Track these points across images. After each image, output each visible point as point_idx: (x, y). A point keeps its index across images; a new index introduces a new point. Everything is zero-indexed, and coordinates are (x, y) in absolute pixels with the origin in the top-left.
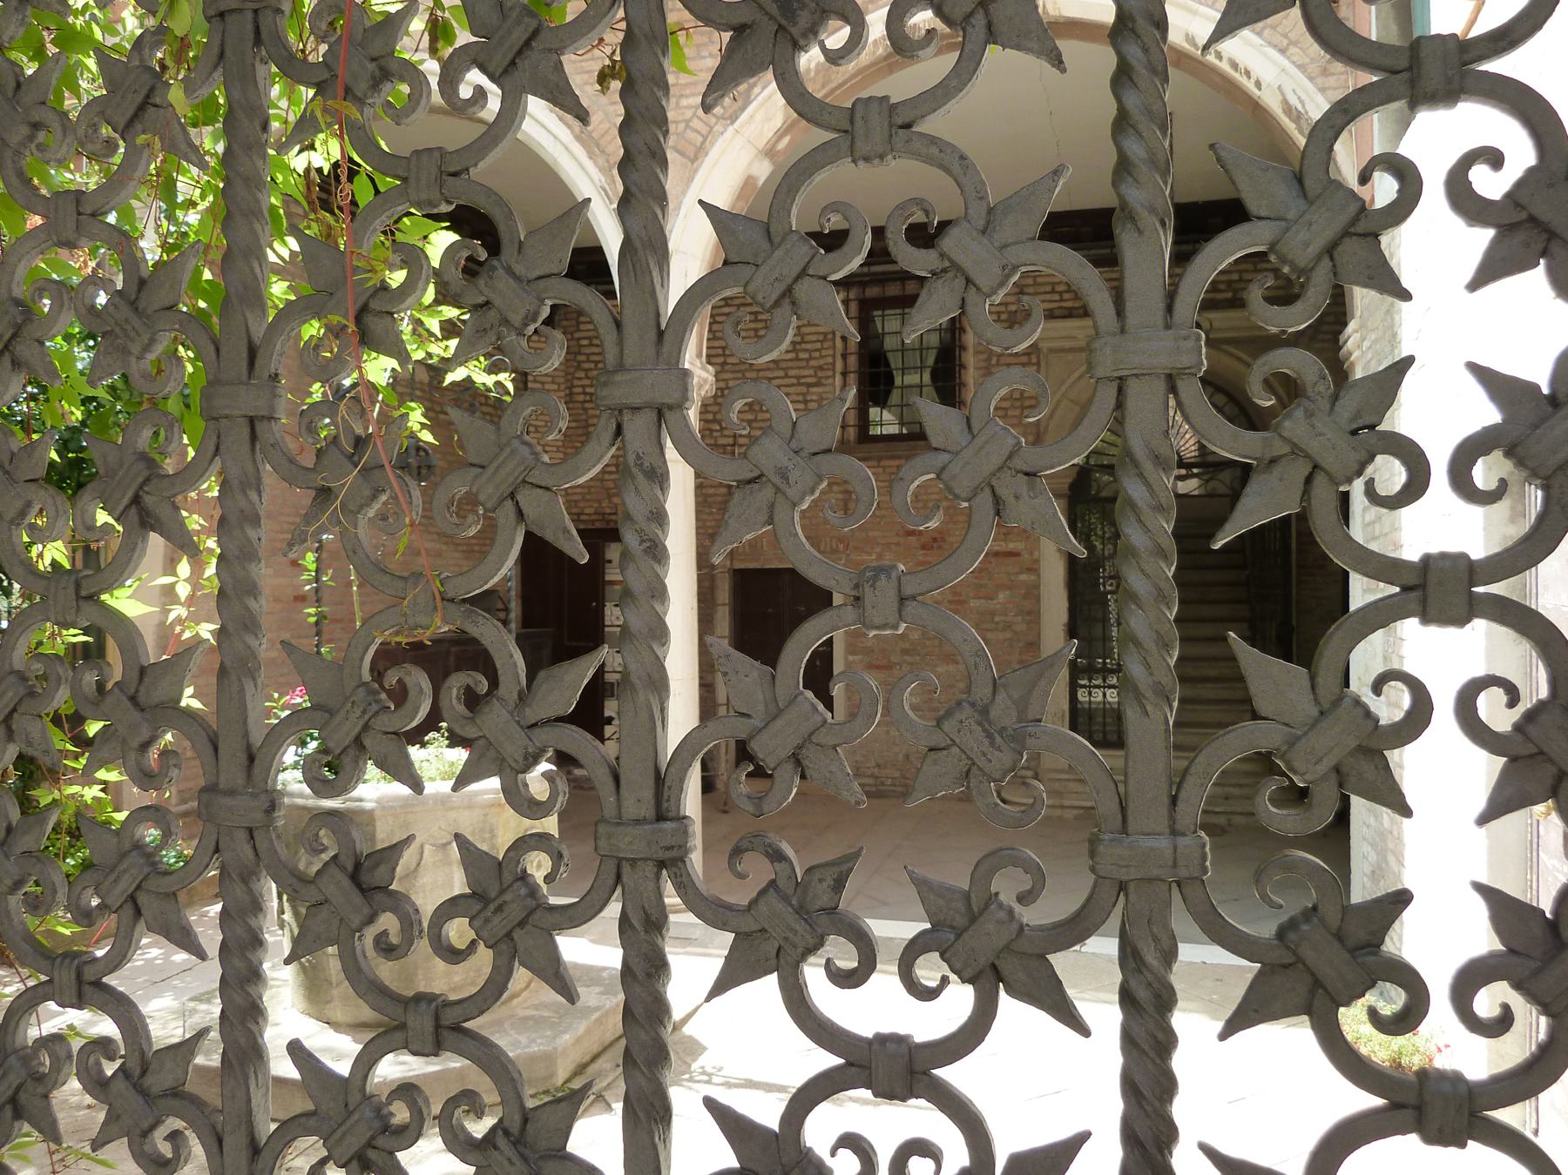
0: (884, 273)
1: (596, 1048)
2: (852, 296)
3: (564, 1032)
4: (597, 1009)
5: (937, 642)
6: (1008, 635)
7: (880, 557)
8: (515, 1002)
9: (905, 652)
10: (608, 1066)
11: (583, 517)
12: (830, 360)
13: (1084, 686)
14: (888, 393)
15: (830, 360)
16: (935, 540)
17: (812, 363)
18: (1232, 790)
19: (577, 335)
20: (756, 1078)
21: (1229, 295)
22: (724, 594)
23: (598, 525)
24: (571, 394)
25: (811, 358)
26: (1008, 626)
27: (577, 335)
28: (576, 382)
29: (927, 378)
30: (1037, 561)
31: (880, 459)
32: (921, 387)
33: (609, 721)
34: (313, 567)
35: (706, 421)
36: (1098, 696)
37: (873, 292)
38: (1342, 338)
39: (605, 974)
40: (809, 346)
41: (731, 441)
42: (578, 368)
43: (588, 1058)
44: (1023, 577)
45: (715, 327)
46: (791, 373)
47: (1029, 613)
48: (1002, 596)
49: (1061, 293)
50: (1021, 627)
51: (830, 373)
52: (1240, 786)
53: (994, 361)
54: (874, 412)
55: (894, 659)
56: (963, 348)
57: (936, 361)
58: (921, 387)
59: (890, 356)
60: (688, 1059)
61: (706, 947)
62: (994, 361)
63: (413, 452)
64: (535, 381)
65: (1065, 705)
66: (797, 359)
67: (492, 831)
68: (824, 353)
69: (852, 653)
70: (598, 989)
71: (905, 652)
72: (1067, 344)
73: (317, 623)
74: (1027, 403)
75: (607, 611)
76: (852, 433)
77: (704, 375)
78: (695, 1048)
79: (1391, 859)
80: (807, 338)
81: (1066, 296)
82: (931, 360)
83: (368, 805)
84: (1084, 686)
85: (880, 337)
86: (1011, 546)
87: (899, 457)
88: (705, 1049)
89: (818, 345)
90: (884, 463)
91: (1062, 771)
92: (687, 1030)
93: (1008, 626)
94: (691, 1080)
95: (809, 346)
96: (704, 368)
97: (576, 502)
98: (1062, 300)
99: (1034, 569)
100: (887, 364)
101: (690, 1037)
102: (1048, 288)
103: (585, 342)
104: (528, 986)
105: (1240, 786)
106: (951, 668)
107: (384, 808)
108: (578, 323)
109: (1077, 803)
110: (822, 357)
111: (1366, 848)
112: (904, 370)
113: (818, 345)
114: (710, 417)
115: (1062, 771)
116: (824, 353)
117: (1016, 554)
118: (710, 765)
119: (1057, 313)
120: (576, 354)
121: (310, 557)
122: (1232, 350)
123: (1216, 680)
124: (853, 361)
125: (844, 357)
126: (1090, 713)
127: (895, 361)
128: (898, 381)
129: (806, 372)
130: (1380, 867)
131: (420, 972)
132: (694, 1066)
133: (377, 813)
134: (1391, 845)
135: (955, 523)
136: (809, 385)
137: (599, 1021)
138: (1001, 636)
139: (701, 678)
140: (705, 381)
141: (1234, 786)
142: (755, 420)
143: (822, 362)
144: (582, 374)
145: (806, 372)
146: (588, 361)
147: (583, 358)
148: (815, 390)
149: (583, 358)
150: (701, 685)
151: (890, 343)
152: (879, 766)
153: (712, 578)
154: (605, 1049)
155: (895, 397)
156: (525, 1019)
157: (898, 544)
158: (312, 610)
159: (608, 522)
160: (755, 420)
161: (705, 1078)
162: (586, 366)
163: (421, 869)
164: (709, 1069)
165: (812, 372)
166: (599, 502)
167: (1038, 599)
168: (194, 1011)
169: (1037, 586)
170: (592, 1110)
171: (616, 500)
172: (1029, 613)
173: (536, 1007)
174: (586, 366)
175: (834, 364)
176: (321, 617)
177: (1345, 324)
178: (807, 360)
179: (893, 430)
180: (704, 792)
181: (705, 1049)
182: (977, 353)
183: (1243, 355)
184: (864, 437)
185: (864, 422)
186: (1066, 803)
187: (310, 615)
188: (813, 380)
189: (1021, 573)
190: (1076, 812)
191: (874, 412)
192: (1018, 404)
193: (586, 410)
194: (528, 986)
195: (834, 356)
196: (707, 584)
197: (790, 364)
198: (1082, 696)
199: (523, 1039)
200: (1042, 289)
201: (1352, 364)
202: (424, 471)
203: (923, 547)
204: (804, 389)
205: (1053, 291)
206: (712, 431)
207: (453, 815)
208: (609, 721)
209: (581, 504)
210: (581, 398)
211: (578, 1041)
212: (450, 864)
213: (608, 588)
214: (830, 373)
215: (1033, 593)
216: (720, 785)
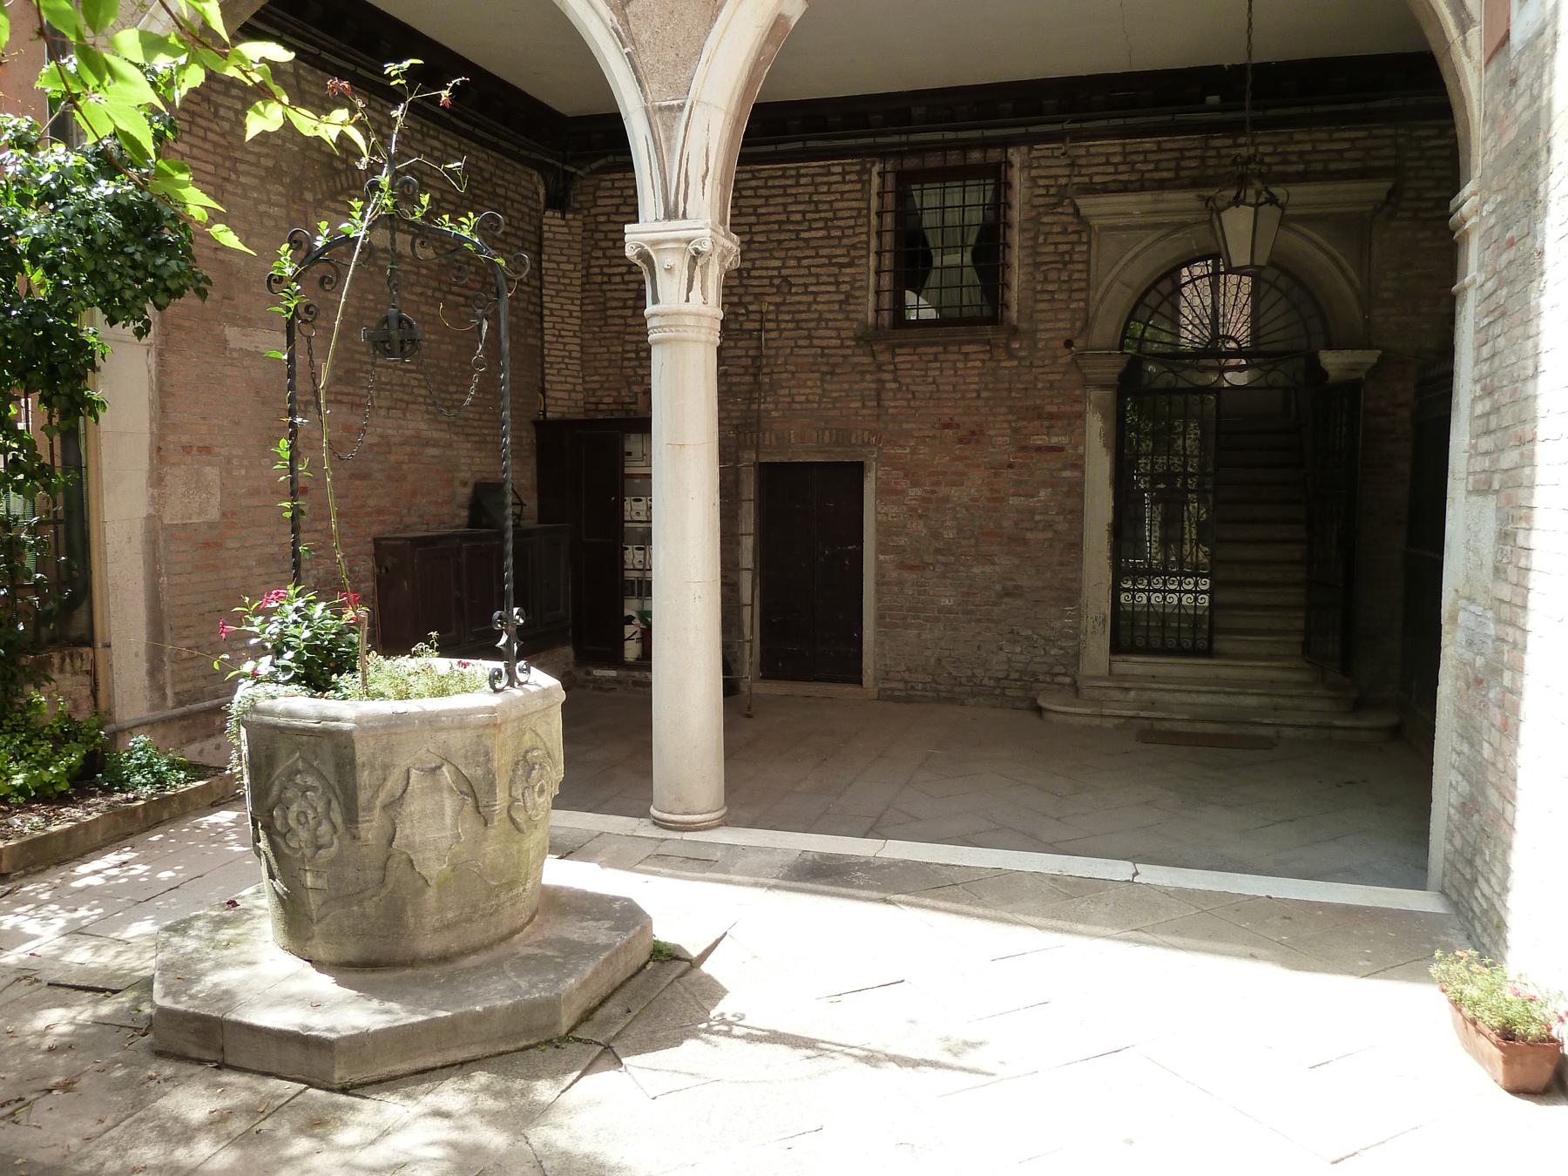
0: (924, 142)
1: (604, 991)
2: (889, 167)
3: (569, 976)
4: (606, 947)
5: (973, 541)
6: (1050, 535)
7: (914, 451)
8: (517, 937)
9: (938, 551)
10: (618, 1011)
11: (602, 407)
12: (864, 238)
13: (1127, 590)
14: (925, 275)
15: (864, 238)
16: (973, 433)
17: (845, 241)
18: (1281, 701)
19: (593, 211)
20: (783, 1028)
21: (1301, 167)
22: (749, 489)
23: (616, 415)
24: (588, 275)
25: (844, 236)
26: (1049, 525)
27: (593, 211)
28: (593, 262)
29: (968, 258)
30: (1082, 457)
31: (916, 345)
32: (962, 267)
33: (630, 620)
34: (287, 455)
35: (731, 304)
36: (1156, 598)
37: (911, 163)
38: (1453, 204)
39: (617, 906)
40: (841, 223)
41: (757, 325)
42: (596, 247)
43: (596, 1002)
44: (1066, 474)
45: (741, 202)
46: (822, 252)
47: (1071, 512)
48: (1043, 494)
49: (1115, 165)
50: (1062, 527)
51: (863, 252)
52: (1291, 696)
53: (1041, 240)
54: (911, 298)
55: (929, 559)
56: (1008, 225)
57: (979, 240)
58: (962, 267)
59: (929, 233)
60: (706, 1004)
61: (728, 872)
62: (1041, 240)
63: (394, 323)
64: (549, 261)
65: (1107, 609)
66: (829, 237)
67: (487, 754)
68: (858, 230)
69: (883, 553)
70: (607, 924)
71: (938, 551)
72: (1122, 221)
73: (293, 518)
74: (1076, 286)
75: (627, 506)
76: (886, 317)
77: (729, 244)
78: (714, 991)
79: (1493, 794)
80: (840, 214)
81: (1122, 168)
82: (972, 240)
83: (347, 726)
84: (1127, 590)
85: (917, 214)
86: (1054, 440)
87: (936, 344)
88: (725, 992)
89: (852, 222)
90: (921, 350)
91: (1102, 678)
92: (706, 968)
93: (1049, 525)
94: (708, 1031)
95: (841, 223)
96: (727, 237)
97: (594, 390)
98: (1116, 173)
99: (1078, 464)
100: (925, 243)
101: (709, 977)
102: (1103, 160)
103: (602, 219)
104: (531, 919)
105: (1291, 696)
106: (988, 569)
107: (363, 729)
108: (595, 199)
109: (1118, 712)
110: (855, 235)
111: (1454, 777)
112: (944, 250)
113: (852, 222)
114: (735, 299)
115: (1102, 678)
116: (858, 230)
117: (1058, 449)
118: (733, 667)
119: (1112, 186)
120: (593, 231)
121: (284, 444)
122: (1305, 230)
123: (1266, 584)
124: (888, 238)
125: (879, 234)
126: (1133, 616)
127: (933, 239)
128: (937, 262)
129: (839, 252)
130: (1473, 799)
131: (409, 908)
132: (714, 1013)
133: (355, 734)
134: (1492, 778)
135: (994, 415)
136: (841, 266)
137: (608, 961)
138: (1041, 536)
139: (722, 576)
140: (730, 251)
141: (1284, 696)
142: (783, 303)
143: (856, 240)
144: (600, 253)
145: (839, 252)
146: (606, 239)
147: (601, 236)
148: (848, 270)
149: (601, 236)
150: (723, 584)
151: (930, 219)
152: (909, 670)
153: (737, 472)
154: (615, 991)
155: (933, 278)
156: (528, 957)
157: (933, 437)
158: (287, 504)
159: (628, 412)
160: (783, 303)
161: (725, 1028)
162: (604, 244)
163: (407, 797)
164: (729, 1018)
165: (844, 251)
166: (618, 390)
167: (1081, 496)
168: (165, 945)
169: (1080, 483)
170: (601, 1063)
171: (635, 388)
172: (1071, 512)
173: (539, 945)
174: (604, 244)
175: (868, 243)
176: (297, 512)
177: (1456, 189)
178: (840, 238)
179: (929, 314)
180: (725, 695)
181: (725, 992)
182: (1022, 230)
183: (1315, 236)
184: (899, 320)
185: (899, 306)
186: (1107, 712)
187: (286, 509)
188: (846, 260)
189: (1065, 469)
190: (1116, 721)
191: (911, 298)
192: (1065, 286)
193: (604, 292)
194: (531, 919)
195: (868, 234)
196: (731, 478)
197: (821, 243)
198: (1124, 598)
199: (523, 984)
200: (1096, 160)
201: (1466, 233)
202: (407, 348)
203: (960, 441)
204: (835, 270)
205: (1107, 163)
206: (737, 315)
207: (443, 736)
208: (630, 620)
209: (599, 393)
210: (599, 279)
211: (584, 984)
212: (441, 790)
213: (627, 481)
214: (863, 252)
215: (1076, 490)
216: (744, 687)
